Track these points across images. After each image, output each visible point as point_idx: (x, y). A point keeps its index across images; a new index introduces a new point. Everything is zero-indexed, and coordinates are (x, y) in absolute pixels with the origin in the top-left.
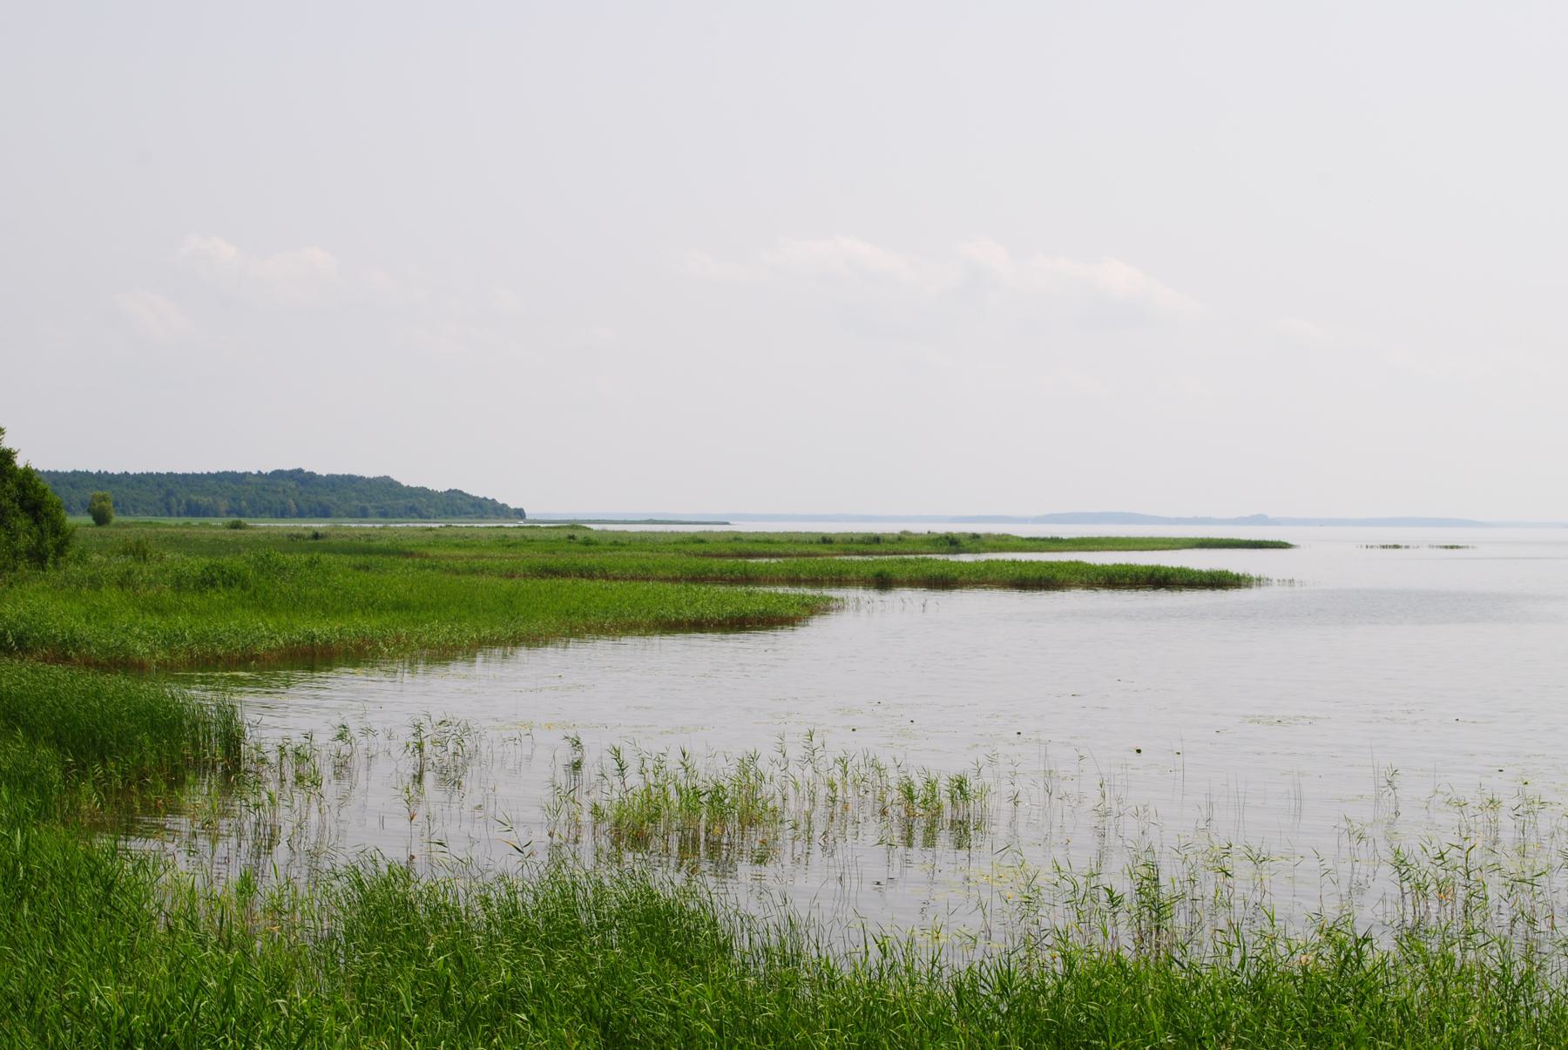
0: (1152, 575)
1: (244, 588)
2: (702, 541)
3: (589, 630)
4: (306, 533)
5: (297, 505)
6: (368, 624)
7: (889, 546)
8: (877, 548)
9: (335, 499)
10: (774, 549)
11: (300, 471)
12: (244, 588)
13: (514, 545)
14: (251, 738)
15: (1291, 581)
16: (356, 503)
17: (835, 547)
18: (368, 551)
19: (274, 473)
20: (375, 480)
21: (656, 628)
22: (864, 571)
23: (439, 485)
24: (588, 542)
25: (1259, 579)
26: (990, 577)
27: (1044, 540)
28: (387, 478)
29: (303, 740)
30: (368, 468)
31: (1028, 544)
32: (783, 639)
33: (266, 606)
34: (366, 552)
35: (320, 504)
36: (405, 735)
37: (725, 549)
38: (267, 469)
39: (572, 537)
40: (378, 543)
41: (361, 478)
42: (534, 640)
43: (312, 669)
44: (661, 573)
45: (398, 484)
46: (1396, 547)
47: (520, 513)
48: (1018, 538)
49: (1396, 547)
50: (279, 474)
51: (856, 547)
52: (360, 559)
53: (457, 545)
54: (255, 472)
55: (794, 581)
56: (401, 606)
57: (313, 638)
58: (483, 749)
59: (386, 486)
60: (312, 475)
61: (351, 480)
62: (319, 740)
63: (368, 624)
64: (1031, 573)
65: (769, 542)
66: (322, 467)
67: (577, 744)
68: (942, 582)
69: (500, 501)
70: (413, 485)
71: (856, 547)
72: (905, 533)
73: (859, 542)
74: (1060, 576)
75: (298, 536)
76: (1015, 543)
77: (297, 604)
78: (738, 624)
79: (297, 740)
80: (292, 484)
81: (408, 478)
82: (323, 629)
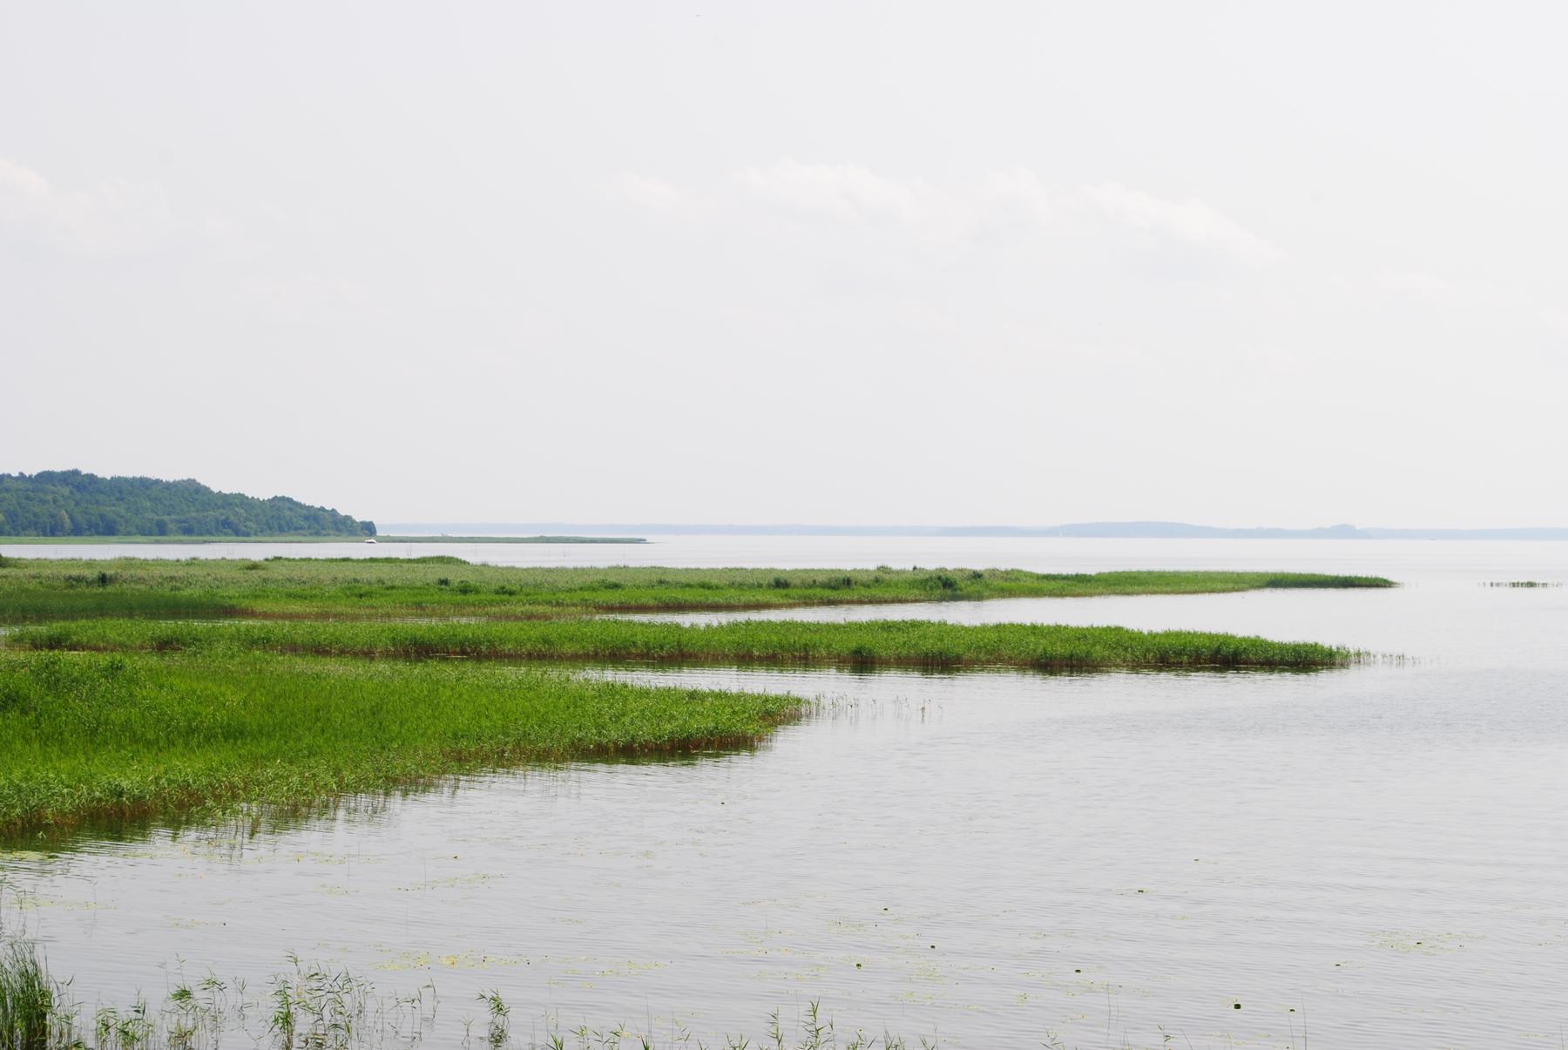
0: (1218, 650)
1: (24, 712)
2: (616, 586)
3: (485, 760)
4: (87, 573)
5: (72, 518)
6: (188, 767)
7: (865, 592)
8: (844, 594)
9: (122, 511)
10: (713, 597)
11: (76, 473)
12: (24, 712)
13: (369, 594)
14: (61, 1004)
15: (1401, 657)
16: (150, 515)
17: (793, 592)
18: (176, 609)
19: (40, 475)
20: (176, 484)
21: (572, 758)
22: (836, 647)
23: (261, 491)
24: (465, 590)
25: (1358, 654)
26: (1006, 652)
27: (1066, 578)
28: (191, 482)
29: (134, 1015)
30: (168, 470)
31: (1052, 585)
32: (740, 764)
33: (51, 738)
34: (177, 609)
35: (102, 516)
36: (270, 1006)
37: (647, 598)
38: (32, 470)
39: (445, 582)
40: (187, 592)
41: (158, 482)
42: (412, 783)
43: (120, 839)
44: (568, 648)
45: (207, 489)
46: (1531, 585)
47: (368, 529)
48: (1031, 575)
49: (1531, 585)
50: (47, 477)
51: (819, 592)
52: (166, 627)
53: (289, 595)
54: (15, 474)
55: (744, 659)
56: (234, 733)
57: (120, 794)
58: (371, 1005)
59: (191, 492)
60: (91, 477)
61: (144, 486)
62: (152, 1014)
63: (188, 767)
64: (1060, 650)
65: (705, 586)
66: (105, 467)
67: (499, 1008)
68: (940, 658)
69: (342, 512)
70: (226, 491)
71: (819, 592)
72: (883, 569)
73: (825, 586)
74: (1098, 652)
75: (79, 579)
76: (1029, 583)
77: (94, 735)
78: (681, 749)
79: (125, 1013)
80: (66, 491)
81: (220, 482)
82: (132, 777)
